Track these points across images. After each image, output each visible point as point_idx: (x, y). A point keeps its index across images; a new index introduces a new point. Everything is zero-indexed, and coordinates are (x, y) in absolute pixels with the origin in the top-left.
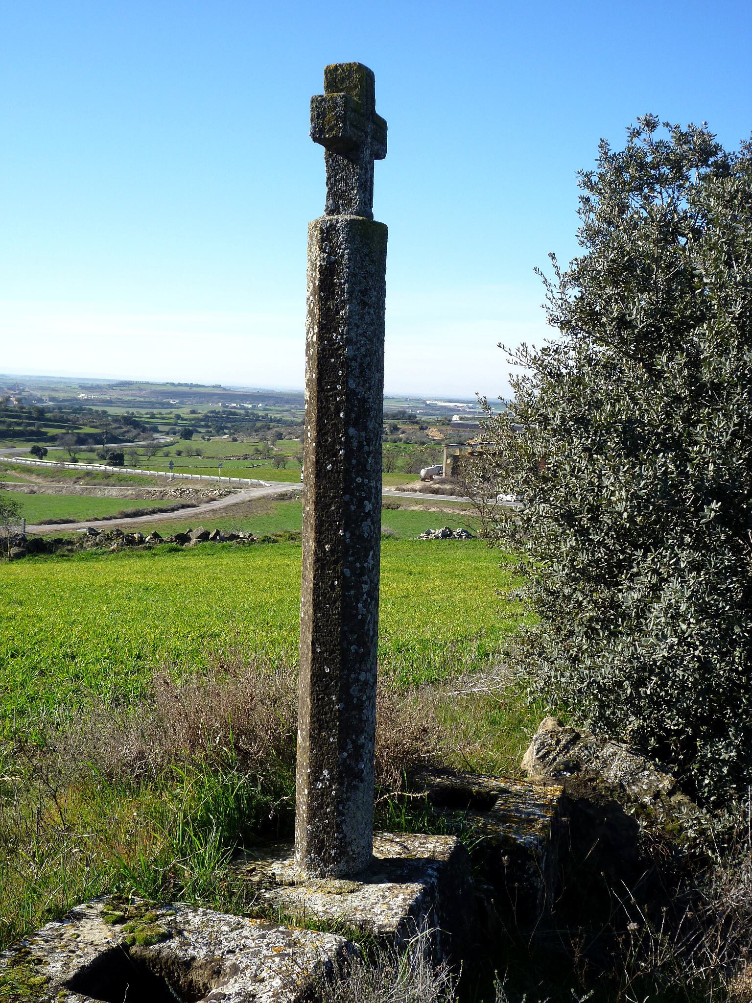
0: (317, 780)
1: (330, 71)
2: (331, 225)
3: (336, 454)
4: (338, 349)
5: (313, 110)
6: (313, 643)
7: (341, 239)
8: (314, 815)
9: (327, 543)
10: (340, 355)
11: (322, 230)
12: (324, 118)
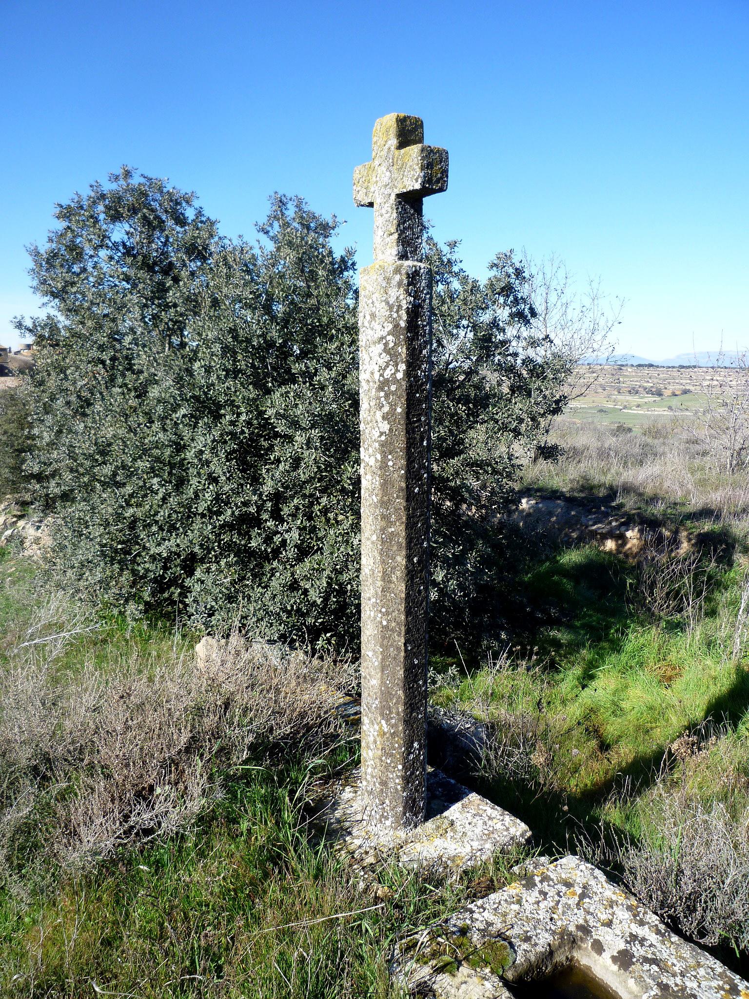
0: (409, 753)
1: (401, 120)
2: (416, 271)
3: (420, 479)
4: (422, 384)
5: (423, 159)
6: (405, 644)
7: (423, 284)
8: (408, 782)
9: (415, 556)
10: (424, 390)
11: (408, 274)
12: (432, 168)
